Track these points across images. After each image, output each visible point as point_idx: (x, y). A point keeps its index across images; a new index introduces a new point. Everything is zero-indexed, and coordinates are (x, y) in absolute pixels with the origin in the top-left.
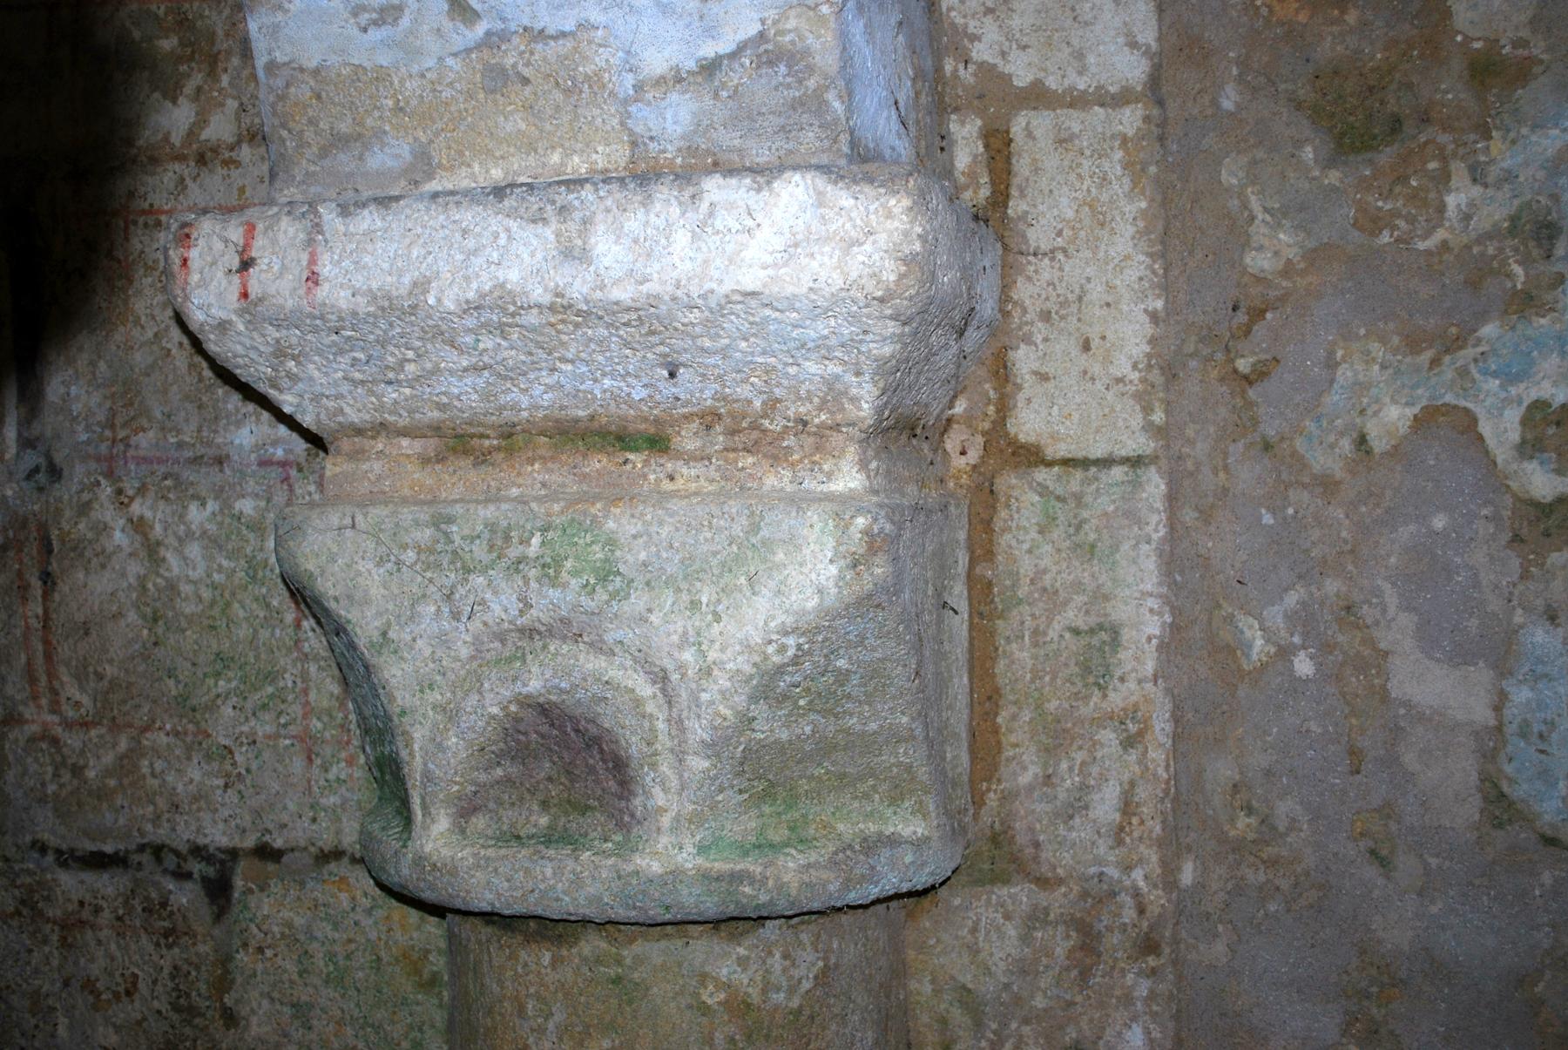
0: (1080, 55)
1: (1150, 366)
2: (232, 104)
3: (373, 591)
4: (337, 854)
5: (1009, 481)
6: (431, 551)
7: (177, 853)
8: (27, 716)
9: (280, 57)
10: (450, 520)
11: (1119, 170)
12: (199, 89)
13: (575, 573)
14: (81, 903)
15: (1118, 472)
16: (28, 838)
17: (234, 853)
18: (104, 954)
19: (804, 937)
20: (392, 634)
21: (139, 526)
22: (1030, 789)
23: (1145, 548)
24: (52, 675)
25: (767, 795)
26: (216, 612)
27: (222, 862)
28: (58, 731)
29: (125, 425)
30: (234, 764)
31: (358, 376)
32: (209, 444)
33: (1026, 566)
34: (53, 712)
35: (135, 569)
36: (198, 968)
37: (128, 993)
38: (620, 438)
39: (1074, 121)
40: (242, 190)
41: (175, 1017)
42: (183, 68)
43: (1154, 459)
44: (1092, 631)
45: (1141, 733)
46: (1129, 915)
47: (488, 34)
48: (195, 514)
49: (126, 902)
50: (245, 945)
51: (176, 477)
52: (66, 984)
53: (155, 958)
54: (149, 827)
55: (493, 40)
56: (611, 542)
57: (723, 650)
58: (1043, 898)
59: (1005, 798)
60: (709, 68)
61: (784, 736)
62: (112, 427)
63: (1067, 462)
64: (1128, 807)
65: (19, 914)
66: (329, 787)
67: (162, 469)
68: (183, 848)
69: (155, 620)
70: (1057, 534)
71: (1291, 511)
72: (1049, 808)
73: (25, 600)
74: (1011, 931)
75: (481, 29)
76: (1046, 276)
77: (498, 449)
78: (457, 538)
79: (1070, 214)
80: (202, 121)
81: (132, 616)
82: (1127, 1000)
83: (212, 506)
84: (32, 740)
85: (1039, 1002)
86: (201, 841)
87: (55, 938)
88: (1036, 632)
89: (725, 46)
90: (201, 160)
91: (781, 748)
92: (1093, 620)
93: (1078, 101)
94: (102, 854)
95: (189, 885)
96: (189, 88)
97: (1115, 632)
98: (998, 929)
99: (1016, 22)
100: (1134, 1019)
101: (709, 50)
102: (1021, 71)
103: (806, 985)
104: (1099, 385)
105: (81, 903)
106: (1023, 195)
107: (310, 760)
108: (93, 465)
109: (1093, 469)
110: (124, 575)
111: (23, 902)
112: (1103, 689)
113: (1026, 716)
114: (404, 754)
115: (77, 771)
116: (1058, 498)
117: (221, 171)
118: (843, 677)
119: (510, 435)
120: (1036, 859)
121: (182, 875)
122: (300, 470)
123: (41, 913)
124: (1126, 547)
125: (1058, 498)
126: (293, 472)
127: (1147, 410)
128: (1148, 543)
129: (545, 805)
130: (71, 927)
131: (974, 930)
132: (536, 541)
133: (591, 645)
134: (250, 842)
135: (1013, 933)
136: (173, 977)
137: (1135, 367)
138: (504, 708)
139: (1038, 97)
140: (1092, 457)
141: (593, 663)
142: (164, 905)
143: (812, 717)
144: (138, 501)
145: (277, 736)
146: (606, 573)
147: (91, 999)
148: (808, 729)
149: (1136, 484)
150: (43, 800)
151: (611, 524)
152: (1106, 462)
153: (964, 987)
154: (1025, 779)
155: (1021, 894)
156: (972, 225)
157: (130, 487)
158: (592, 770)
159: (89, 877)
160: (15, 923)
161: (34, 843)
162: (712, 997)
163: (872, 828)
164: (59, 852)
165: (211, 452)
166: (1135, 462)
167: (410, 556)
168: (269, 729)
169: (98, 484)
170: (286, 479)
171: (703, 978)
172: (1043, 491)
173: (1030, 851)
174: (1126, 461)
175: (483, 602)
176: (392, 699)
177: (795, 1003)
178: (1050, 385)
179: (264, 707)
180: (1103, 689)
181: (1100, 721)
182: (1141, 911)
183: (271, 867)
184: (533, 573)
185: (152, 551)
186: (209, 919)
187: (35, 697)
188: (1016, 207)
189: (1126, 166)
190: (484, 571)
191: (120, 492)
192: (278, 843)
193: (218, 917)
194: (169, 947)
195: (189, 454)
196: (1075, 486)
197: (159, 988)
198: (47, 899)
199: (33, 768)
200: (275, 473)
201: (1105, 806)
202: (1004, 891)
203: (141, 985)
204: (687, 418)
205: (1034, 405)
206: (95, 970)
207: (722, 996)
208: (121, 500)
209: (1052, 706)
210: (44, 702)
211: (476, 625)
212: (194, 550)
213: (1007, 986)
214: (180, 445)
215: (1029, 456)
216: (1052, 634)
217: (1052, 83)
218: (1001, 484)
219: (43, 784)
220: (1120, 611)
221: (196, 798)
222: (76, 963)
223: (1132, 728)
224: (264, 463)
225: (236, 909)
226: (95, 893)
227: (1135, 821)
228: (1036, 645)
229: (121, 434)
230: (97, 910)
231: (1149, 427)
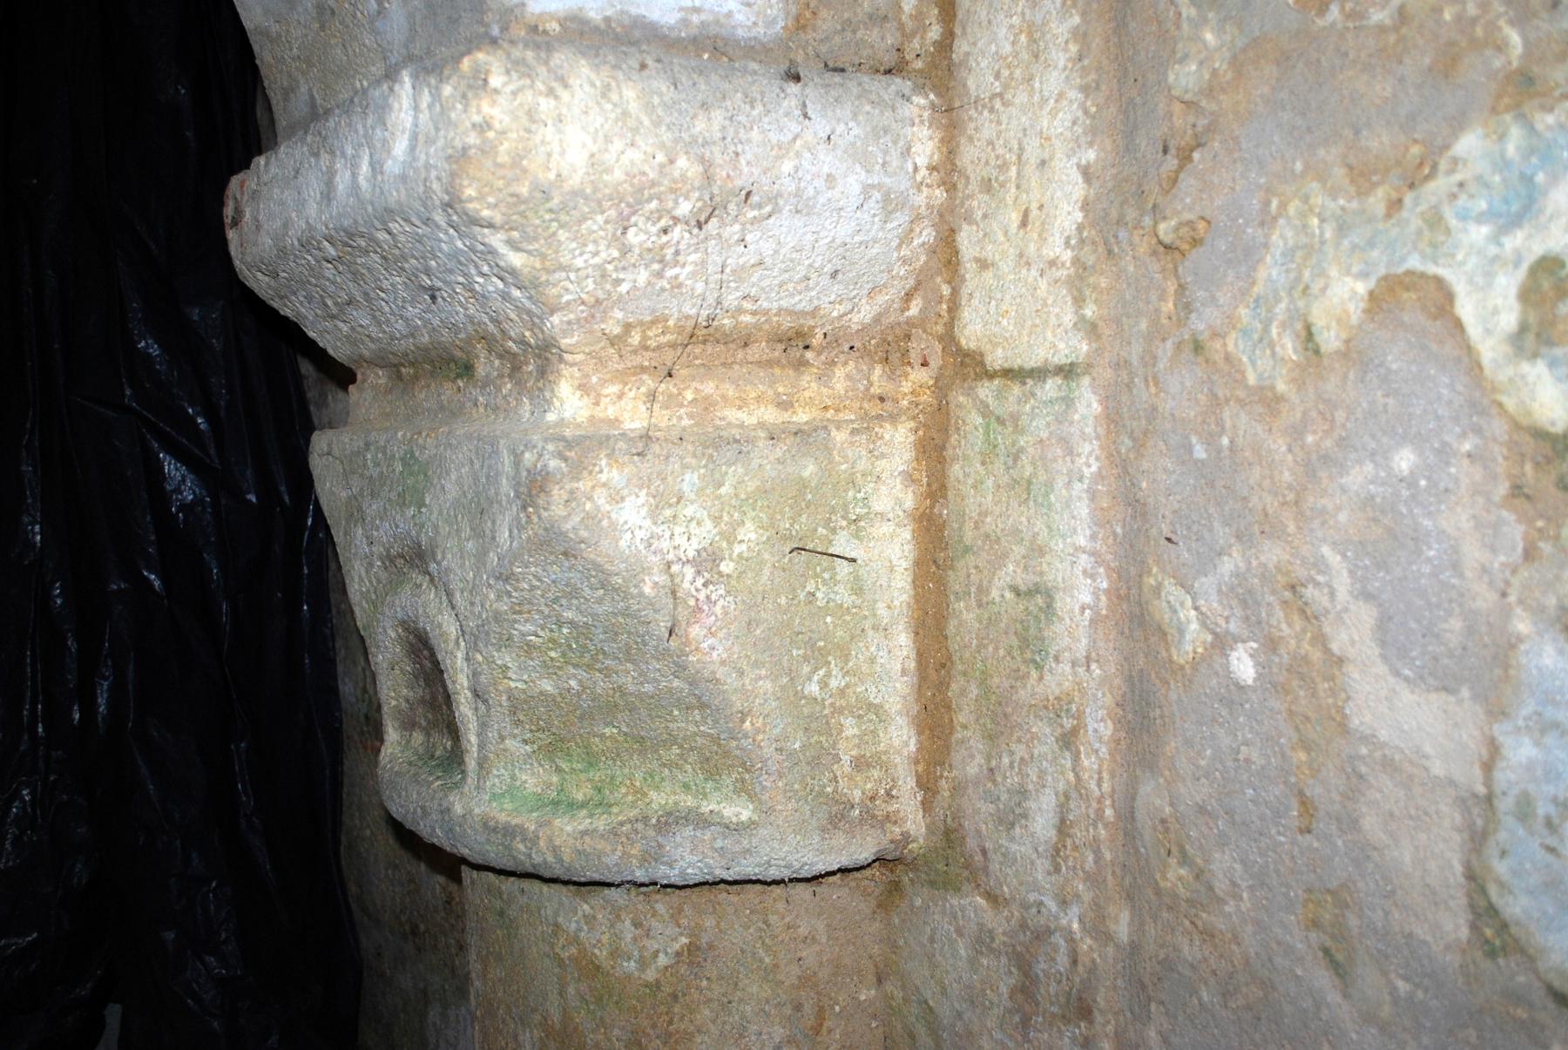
1: (1082, 241)
15: (1051, 387)
19: (660, 907)
23: (1077, 486)
46: (1063, 961)
64: (1063, 827)
70: (999, 467)
71: (1225, 441)
103: (662, 960)
106: (964, 33)
127: (1079, 301)
128: (1080, 480)
152: (1039, 374)
166: (1067, 372)
172: (985, 410)
173: (978, 858)
177: (650, 975)
216: (995, 594)
223: (1068, 723)
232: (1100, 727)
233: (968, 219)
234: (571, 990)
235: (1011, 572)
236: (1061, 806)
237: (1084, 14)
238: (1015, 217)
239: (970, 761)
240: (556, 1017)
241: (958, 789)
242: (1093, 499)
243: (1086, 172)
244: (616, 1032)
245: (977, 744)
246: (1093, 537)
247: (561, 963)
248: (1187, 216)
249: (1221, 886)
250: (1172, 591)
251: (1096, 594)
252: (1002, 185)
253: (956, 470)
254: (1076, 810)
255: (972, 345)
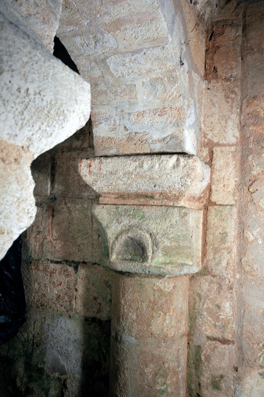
0: (225, 138)
1: (235, 190)
2: (88, 142)
3: (106, 218)
4: (95, 264)
5: (210, 208)
6: (115, 212)
7: (70, 262)
8: (48, 238)
9: (98, 135)
10: (119, 208)
11: (231, 157)
12: (82, 139)
13: (138, 217)
14: (54, 269)
15: (228, 207)
16: (46, 258)
17: (79, 262)
18: (57, 278)
19: (171, 280)
20: (108, 225)
21: (68, 208)
22: (211, 260)
24: (52, 232)
25: (166, 255)
26: (79, 222)
27: (77, 264)
28: (52, 241)
29: (67, 191)
30: (80, 248)
31: (106, 184)
32: (80, 195)
33: (212, 222)
34: (52, 237)
35: (67, 215)
36: (71, 281)
37: (60, 285)
38: (146, 196)
39: (223, 149)
40: (88, 155)
41: (67, 289)
42: (80, 136)
43: (235, 205)
44: (223, 234)
45: (231, 251)
46: (227, 282)
47: (130, 132)
48: (77, 207)
49: (61, 270)
50: (80, 278)
51: (75, 200)
52: (50, 282)
53: (65, 279)
54: (66, 257)
55: (130, 134)
56: (144, 212)
57: (160, 230)
58: (213, 279)
59: (207, 261)
60: (164, 139)
61: (169, 245)
62: (65, 192)
63: (220, 205)
64: (228, 264)
65: (44, 270)
66: (95, 252)
67: (72, 199)
68: (71, 261)
69: (69, 223)
70: (218, 217)
72: (214, 263)
73: (49, 219)
74: (207, 284)
75: (128, 132)
76: (218, 174)
77: (127, 197)
78: (119, 211)
79: (222, 164)
80: (83, 144)
81: (66, 222)
82: (226, 297)
83: (80, 205)
84: (48, 242)
85: (211, 297)
86: (74, 260)
87: (49, 275)
88: (213, 233)
89: (166, 135)
90: (82, 150)
91: (169, 247)
92: (223, 232)
93: (224, 145)
94: (58, 261)
95: (71, 267)
96: (81, 139)
97: (227, 234)
98: (205, 283)
99: (215, 132)
100: (228, 301)
101: (164, 136)
102: (215, 140)
103: (171, 288)
104: (226, 192)
105: (54, 269)
106: (214, 160)
107: (92, 248)
108: (61, 198)
109: (224, 206)
110: (65, 216)
111: (44, 269)
112: (224, 243)
113: (211, 247)
114: (109, 245)
115: (55, 247)
116: (218, 211)
117: (85, 152)
118: (179, 236)
119: (129, 195)
120: (212, 272)
121: (70, 266)
122: (94, 200)
123: (47, 271)
124: (229, 220)
125: (218, 211)
126: (93, 201)
127: (234, 197)
129: (131, 254)
130: (52, 273)
131: (201, 283)
132: (132, 212)
133: (140, 229)
134: (81, 261)
135: (207, 284)
136: (67, 282)
137: (232, 189)
138: (125, 238)
139: (218, 145)
140: (224, 204)
141: (140, 232)
142: (67, 270)
143: (174, 242)
144: (68, 204)
145: (87, 244)
146: (143, 217)
147: (54, 285)
148: (173, 244)
149: (231, 209)
150: (49, 252)
151: (144, 209)
152: (227, 205)
153: (199, 293)
154: (210, 258)
155: (209, 277)
156: (205, 165)
157: (67, 201)
158: (138, 249)
159: (55, 265)
160: (43, 272)
161: (47, 259)
162: (155, 288)
163: (183, 262)
164: (51, 260)
165: (81, 197)
166: (232, 205)
167: (112, 213)
168: (87, 242)
169: (62, 201)
170: (92, 202)
171: (154, 285)
172: (216, 209)
173: (211, 270)
174: (230, 205)
175: (123, 221)
176: (107, 236)
177: (169, 291)
178: (218, 192)
179: (86, 238)
180: (224, 243)
181: (224, 248)
182: (230, 282)
183: (85, 265)
184: (131, 217)
185: (70, 212)
186: (74, 273)
187: (49, 235)
188: (213, 162)
189: (232, 156)
190: (124, 216)
191: (66, 202)
192: (86, 261)
193: (76, 273)
194: (67, 277)
195: (77, 197)
196: (221, 209)
197: (65, 284)
198: (48, 268)
199: (48, 246)
200: (90, 200)
201: (224, 263)
202: (206, 277)
203: (62, 283)
204: (157, 193)
205: (215, 195)
206: (55, 281)
207: (157, 288)
208: (66, 204)
209: (216, 246)
210: (50, 236)
211: (122, 224)
212: (77, 212)
213: (206, 294)
214: (76, 195)
215: (215, 204)
216: (216, 234)
217: (220, 142)
218: (209, 208)
219: (49, 249)
220: (227, 230)
221: (74, 253)
222: (52, 279)
223: (229, 250)
224: (89, 199)
225: (78, 272)
226: (56, 268)
227: (229, 266)
228: (213, 235)
229: (66, 193)
230: (56, 271)
231: (234, 199)
232: (235, 250)
233: (214, 184)
234: (156, 295)
235: (220, 231)
236: (228, 261)
237: (236, 162)
238: (222, 185)
239: (210, 256)
240: (152, 300)
241: (207, 261)
242: (235, 221)
243: (236, 181)
244: (163, 300)
245: (212, 255)
246: (235, 226)
247: (154, 290)
248: (254, 189)
249: (255, 269)
250: (249, 233)
251: (235, 233)
252: (220, 181)
253: (209, 217)
254: (231, 261)
255: (214, 201)
